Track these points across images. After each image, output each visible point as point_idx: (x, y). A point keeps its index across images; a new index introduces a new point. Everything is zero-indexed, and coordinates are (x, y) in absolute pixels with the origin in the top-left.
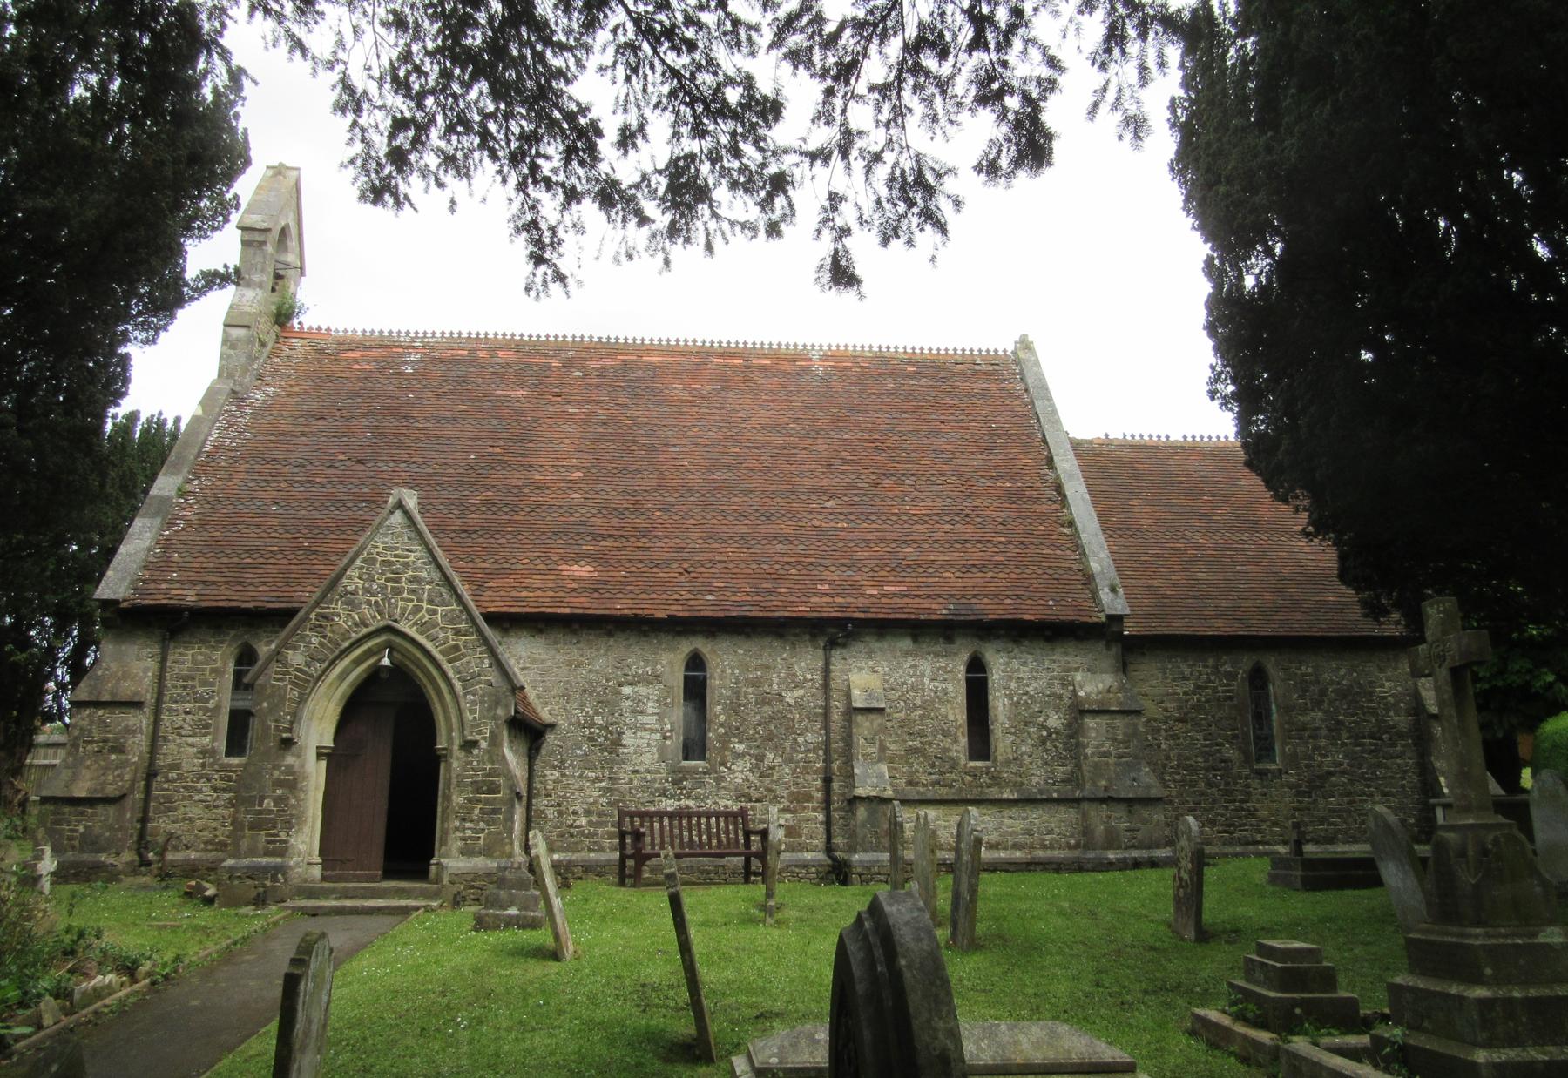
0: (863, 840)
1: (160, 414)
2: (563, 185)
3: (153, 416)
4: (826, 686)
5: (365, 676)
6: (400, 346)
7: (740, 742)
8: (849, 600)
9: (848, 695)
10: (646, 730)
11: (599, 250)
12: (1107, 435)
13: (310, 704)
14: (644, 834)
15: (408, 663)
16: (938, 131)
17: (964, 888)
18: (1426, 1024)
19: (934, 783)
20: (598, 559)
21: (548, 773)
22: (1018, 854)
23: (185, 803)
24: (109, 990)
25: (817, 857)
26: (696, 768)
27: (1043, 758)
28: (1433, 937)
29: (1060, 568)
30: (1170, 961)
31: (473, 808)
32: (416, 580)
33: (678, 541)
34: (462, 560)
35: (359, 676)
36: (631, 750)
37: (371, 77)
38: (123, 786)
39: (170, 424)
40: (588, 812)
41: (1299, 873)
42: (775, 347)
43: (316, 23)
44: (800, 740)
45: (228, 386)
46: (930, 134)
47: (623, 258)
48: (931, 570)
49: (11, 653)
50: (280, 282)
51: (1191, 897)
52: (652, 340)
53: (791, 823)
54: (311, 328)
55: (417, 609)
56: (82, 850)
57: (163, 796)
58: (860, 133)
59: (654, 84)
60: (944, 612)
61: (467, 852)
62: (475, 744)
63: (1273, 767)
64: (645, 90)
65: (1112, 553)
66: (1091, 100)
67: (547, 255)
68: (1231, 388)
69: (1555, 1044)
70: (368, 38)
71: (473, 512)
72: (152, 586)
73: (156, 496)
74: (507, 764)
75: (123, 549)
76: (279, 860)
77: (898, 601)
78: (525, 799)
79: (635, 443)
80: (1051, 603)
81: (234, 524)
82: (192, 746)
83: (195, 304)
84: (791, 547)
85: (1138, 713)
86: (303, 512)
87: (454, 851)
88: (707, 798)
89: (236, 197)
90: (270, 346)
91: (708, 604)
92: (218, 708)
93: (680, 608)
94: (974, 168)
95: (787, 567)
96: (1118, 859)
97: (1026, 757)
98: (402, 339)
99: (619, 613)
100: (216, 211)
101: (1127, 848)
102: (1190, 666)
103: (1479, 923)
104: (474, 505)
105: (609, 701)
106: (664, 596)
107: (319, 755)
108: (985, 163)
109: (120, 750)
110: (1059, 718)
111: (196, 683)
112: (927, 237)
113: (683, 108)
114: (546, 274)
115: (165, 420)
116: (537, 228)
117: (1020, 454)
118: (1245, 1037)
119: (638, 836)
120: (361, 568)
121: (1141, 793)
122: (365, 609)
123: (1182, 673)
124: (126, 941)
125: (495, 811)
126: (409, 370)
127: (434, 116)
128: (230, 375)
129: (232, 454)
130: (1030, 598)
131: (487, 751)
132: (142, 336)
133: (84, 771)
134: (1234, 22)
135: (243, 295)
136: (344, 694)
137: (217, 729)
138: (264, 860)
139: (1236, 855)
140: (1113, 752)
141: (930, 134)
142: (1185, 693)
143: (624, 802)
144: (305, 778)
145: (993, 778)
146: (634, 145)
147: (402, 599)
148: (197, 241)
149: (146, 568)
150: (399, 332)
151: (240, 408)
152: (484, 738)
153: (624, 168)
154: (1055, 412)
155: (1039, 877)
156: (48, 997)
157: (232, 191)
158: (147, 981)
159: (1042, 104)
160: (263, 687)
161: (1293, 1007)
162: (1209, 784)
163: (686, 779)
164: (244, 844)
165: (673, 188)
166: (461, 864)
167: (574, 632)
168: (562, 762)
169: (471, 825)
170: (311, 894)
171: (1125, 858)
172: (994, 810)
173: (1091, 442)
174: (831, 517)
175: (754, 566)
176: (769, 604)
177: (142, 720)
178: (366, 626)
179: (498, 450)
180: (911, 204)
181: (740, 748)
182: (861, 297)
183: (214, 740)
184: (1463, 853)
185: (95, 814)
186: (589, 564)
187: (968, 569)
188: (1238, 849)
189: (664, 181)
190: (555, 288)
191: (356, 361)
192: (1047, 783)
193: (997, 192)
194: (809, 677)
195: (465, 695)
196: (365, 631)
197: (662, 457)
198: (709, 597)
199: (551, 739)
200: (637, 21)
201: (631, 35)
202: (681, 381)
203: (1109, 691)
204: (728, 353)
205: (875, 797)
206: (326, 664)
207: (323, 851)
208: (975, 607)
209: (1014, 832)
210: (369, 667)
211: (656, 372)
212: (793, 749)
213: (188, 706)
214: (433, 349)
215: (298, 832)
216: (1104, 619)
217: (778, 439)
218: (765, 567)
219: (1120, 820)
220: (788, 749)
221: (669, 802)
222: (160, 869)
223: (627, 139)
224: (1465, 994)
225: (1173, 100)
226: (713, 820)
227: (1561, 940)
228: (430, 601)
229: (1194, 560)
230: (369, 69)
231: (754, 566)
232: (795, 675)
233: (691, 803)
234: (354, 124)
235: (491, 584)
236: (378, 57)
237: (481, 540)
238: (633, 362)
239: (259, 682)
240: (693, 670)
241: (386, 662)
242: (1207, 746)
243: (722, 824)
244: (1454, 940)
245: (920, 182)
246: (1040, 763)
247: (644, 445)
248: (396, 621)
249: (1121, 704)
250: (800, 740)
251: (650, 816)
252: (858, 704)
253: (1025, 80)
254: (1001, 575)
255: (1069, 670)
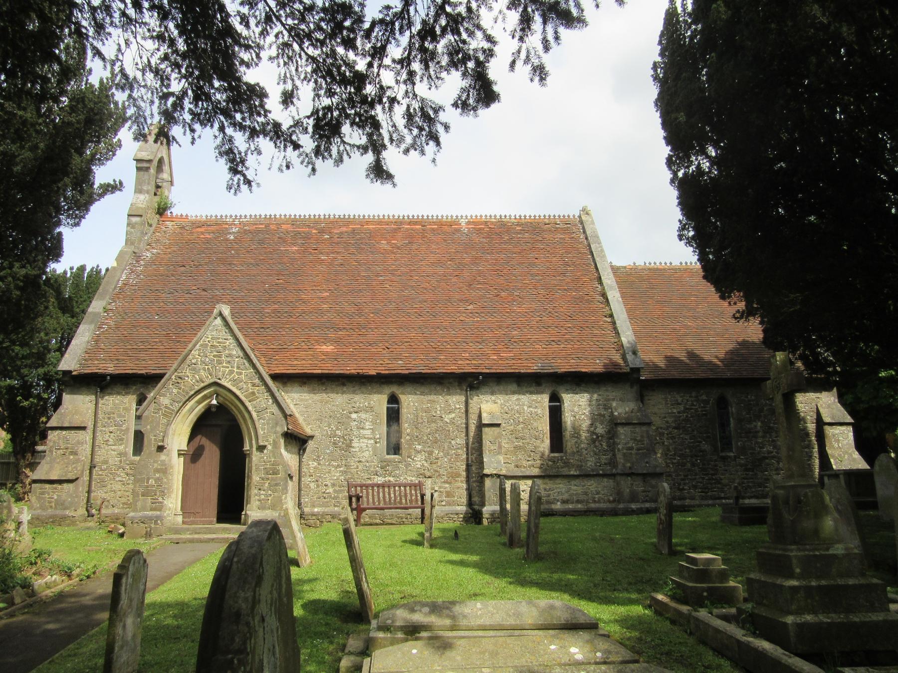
0: (489, 499)
1: (98, 266)
2: (249, 127)
3: (93, 268)
4: (467, 411)
5: (203, 410)
6: (227, 224)
7: (419, 444)
8: (480, 362)
9: (480, 416)
10: (365, 438)
11: (271, 165)
12: (634, 264)
13: (173, 426)
14: (362, 497)
15: (227, 403)
16: (433, 84)
17: (532, 525)
18: (765, 601)
19: (530, 467)
20: (337, 341)
21: (311, 463)
22: (580, 506)
23: (112, 482)
24: (55, 583)
25: (463, 509)
26: (394, 459)
27: (594, 451)
28: (771, 551)
29: (603, 341)
30: (650, 566)
31: (265, 483)
32: (230, 356)
33: (383, 331)
34: (260, 344)
35: (200, 410)
36: (357, 450)
37: (138, 69)
38: (76, 474)
39: (103, 272)
40: (333, 485)
41: (737, 515)
42: (440, 218)
43: (107, 39)
44: (453, 442)
45: (132, 248)
46: (429, 86)
47: (284, 168)
48: (528, 344)
49: (20, 401)
50: (159, 190)
51: (666, 530)
52: (369, 216)
53: (449, 489)
54: (177, 215)
55: (231, 372)
56: (56, 508)
57: (99, 479)
58: (389, 88)
59: (301, 66)
60: (535, 368)
61: (261, 508)
62: (264, 447)
63: (732, 454)
64: (297, 70)
65: (635, 332)
66: (511, 59)
67: (240, 169)
68: (691, 233)
69: (835, 612)
70: (134, 46)
71: (267, 317)
72: (90, 362)
73: (91, 313)
74: (283, 458)
75: (73, 342)
76: (158, 513)
77: (508, 362)
78: (296, 479)
79: (359, 275)
80: (598, 361)
81: (134, 326)
82: (114, 451)
83: (97, 203)
84: (447, 332)
85: (649, 424)
86: (172, 319)
87: (255, 508)
88: (401, 476)
89: (119, 141)
90: (154, 226)
91: (400, 366)
92: (128, 429)
93: (383, 368)
94: (453, 105)
95: (445, 344)
96: (637, 509)
97: (584, 450)
98: (228, 220)
99: (348, 372)
100: (108, 149)
101: (643, 502)
102: (681, 397)
103: (795, 543)
104: (268, 313)
105: (343, 421)
106: (375, 362)
107: (179, 455)
108: (459, 102)
109: (75, 453)
110: (603, 428)
111: (115, 416)
112: (431, 147)
113: (319, 80)
114: (239, 179)
115: (101, 269)
116: (233, 153)
117: (582, 275)
118: (675, 610)
119: (358, 498)
120: (199, 350)
121: (651, 470)
122: (202, 373)
123: (677, 400)
124: (68, 558)
125: (277, 485)
126: (232, 238)
127: (187, 90)
128: (132, 243)
129: (133, 288)
130: (586, 359)
131: (272, 451)
132: (71, 222)
133: (56, 465)
134: (690, 15)
135: (138, 198)
136: (192, 421)
137: (127, 440)
138: (150, 513)
139: (708, 506)
140: (635, 447)
141: (429, 86)
142: (679, 412)
143: (354, 479)
144: (172, 467)
145: (565, 463)
146: (292, 103)
147: (223, 367)
148: (98, 167)
149: (86, 352)
150: (226, 216)
151: (137, 261)
152: (270, 444)
153: (283, 116)
154: (602, 251)
155: (590, 519)
156: (18, 588)
157: (117, 138)
158: (77, 579)
159: (487, 65)
160: (147, 417)
161: (703, 592)
162: (693, 465)
163: (389, 466)
164: (139, 504)
165: (317, 127)
166: (258, 514)
167: (323, 384)
168: (318, 457)
169: (264, 493)
170: (177, 531)
171: (641, 508)
172: (566, 481)
173: (625, 267)
174: (471, 315)
175: (426, 344)
176: (434, 365)
177: (87, 436)
178: (203, 382)
179: (281, 281)
180: (421, 129)
181: (419, 447)
182: (394, 185)
183: (126, 447)
184: (786, 502)
185: (62, 489)
186: (332, 345)
187: (549, 343)
188: (710, 502)
189: (311, 122)
190: (244, 188)
191: (202, 233)
192: (596, 465)
193: (469, 119)
194: (458, 406)
195: (259, 419)
196: (202, 385)
197: (374, 283)
198: (400, 362)
199: (311, 445)
200: (290, 30)
201: (286, 38)
202: (386, 239)
203: (632, 412)
204: (413, 222)
205: (496, 474)
206: (182, 404)
207: (183, 508)
208: (553, 365)
209: (576, 494)
210: (206, 405)
211: (372, 235)
212: (449, 448)
213: (111, 429)
214: (245, 225)
215: (168, 497)
216: (628, 370)
217: (440, 270)
218: (432, 344)
219: (639, 487)
220: (446, 447)
221: (379, 478)
222: (99, 518)
223: (288, 98)
224: (784, 584)
225: (655, 64)
226: (397, 488)
227: (843, 552)
228: (238, 368)
229: (686, 335)
230: (137, 64)
231: (426, 344)
232: (450, 405)
233: (392, 479)
234: (130, 96)
235: (277, 357)
236: (141, 58)
237: (271, 333)
238: (358, 229)
239: (144, 414)
240: (392, 404)
241: (214, 402)
242: (692, 443)
243: (408, 491)
244: (780, 552)
245: (426, 116)
246: (592, 453)
247: (364, 276)
248: (219, 379)
249: (639, 419)
250: (453, 442)
251: (367, 486)
252: (485, 421)
253: (475, 50)
254: (569, 346)
255: (609, 400)
